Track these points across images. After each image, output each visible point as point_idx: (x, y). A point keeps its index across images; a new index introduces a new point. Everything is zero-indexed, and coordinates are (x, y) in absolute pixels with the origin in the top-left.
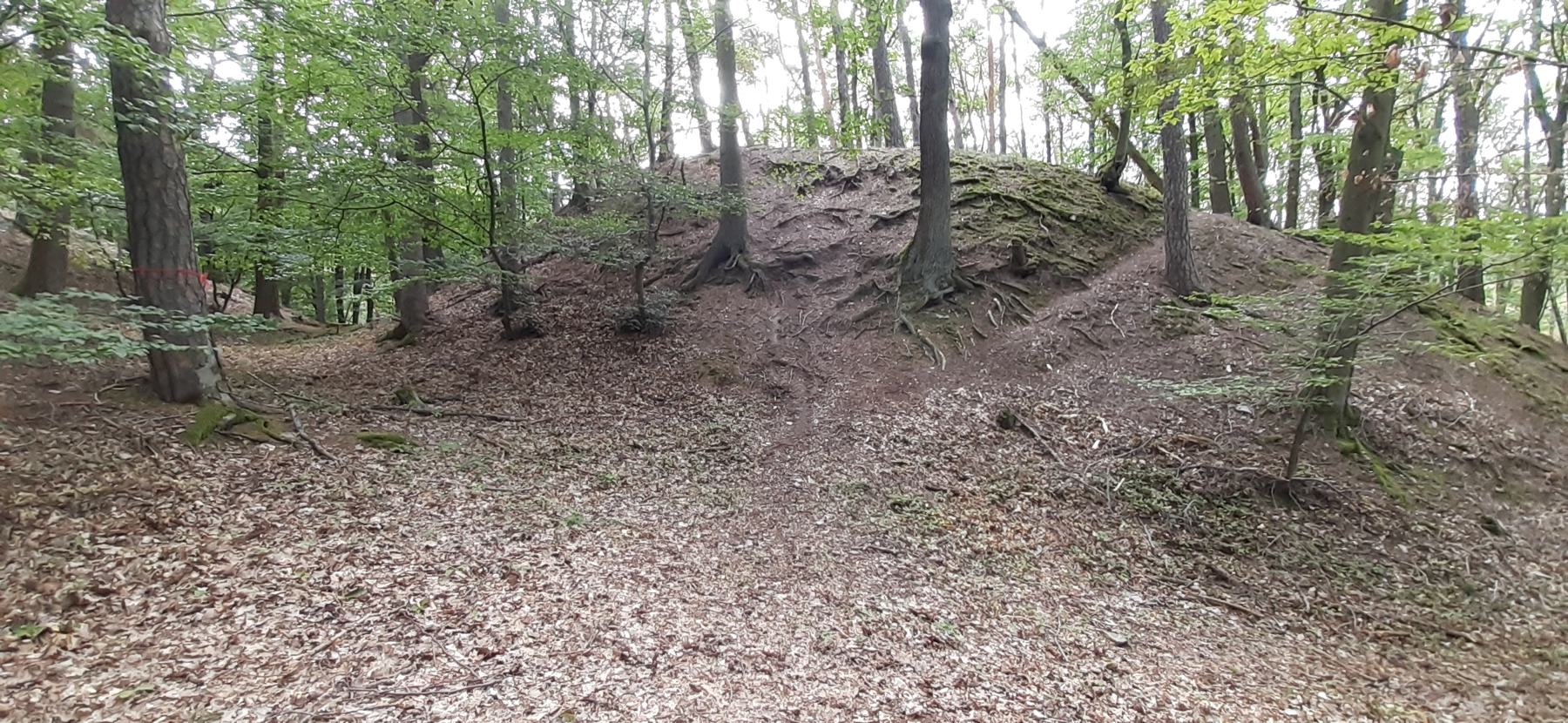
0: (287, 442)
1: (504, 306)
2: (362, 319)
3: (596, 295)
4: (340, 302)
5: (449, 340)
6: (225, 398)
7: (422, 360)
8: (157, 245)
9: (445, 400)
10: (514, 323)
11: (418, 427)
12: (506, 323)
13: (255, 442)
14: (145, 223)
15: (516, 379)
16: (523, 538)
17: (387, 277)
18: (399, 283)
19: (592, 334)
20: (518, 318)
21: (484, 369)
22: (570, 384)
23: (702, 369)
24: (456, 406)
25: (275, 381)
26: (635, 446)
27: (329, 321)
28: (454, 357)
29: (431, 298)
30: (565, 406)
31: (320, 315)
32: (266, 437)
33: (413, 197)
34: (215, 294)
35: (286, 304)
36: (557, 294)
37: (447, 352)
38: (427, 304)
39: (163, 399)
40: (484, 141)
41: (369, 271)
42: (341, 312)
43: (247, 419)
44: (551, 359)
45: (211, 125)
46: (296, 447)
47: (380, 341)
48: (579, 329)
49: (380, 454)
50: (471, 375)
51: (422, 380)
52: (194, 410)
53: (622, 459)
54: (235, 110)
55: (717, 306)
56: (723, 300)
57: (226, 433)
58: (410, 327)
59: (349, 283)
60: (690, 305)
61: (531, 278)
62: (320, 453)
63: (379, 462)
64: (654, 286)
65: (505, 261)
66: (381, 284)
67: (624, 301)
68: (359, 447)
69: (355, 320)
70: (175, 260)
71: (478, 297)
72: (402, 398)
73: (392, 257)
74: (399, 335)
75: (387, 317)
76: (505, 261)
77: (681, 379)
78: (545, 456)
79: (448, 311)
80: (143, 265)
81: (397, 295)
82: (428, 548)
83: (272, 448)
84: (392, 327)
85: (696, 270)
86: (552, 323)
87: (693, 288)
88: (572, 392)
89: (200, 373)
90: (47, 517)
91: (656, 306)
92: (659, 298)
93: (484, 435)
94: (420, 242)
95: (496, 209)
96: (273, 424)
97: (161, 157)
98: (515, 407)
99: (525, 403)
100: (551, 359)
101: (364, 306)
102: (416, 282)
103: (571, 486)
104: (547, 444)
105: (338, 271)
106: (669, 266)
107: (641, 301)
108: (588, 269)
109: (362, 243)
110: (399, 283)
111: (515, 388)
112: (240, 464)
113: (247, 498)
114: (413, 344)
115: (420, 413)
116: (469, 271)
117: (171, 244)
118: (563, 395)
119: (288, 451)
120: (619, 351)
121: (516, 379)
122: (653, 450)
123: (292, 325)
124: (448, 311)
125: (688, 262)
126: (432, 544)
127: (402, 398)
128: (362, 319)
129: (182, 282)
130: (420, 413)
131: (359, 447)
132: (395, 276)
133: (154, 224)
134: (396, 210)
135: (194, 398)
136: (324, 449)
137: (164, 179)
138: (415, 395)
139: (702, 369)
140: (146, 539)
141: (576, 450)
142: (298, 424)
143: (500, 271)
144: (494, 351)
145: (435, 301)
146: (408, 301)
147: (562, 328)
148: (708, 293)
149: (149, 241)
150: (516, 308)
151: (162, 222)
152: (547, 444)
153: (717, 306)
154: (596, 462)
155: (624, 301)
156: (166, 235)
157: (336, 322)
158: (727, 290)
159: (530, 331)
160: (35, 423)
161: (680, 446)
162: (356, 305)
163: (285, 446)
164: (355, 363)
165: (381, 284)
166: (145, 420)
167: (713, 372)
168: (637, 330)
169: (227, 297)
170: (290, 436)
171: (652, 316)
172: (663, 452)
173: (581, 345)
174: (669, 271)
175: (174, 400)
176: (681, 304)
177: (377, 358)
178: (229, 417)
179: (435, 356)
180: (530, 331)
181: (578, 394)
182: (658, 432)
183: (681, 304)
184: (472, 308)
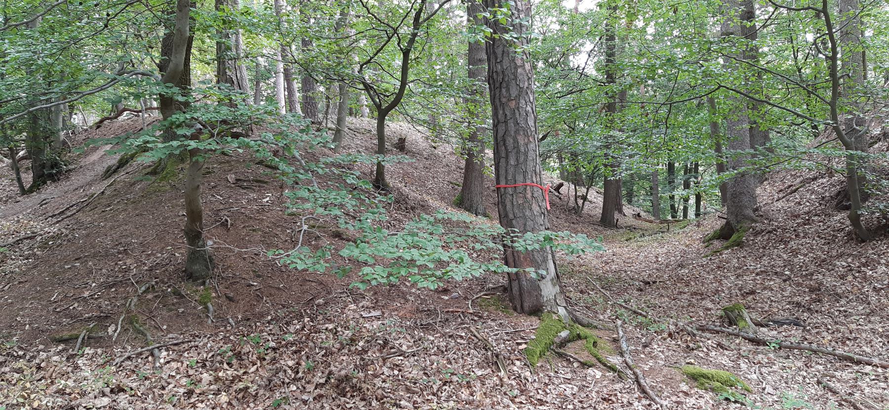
0: (612, 369)
4: (672, 198)
6: (562, 311)
7: (751, 263)
12: (855, 220)
13: (584, 365)
14: (504, 141)
17: (714, 168)
18: (727, 175)
21: (829, 281)
24: (796, 334)
27: (665, 217)
28: (788, 264)
29: (758, 191)
31: (656, 210)
32: (594, 361)
33: (736, 77)
34: (576, 197)
35: (630, 202)
37: (780, 254)
38: (754, 198)
39: (515, 309)
41: (697, 165)
42: (673, 207)
46: (621, 377)
47: (708, 241)
50: (812, 290)
51: (753, 292)
52: (534, 321)
57: (558, 350)
58: (735, 229)
59: (680, 178)
65: (851, 137)
66: (708, 176)
68: (684, 387)
69: (685, 215)
70: (525, 173)
71: (815, 186)
72: (730, 318)
73: (718, 149)
74: (725, 234)
75: (715, 215)
76: (851, 137)
79: (779, 204)
81: (723, 187)
83: (599, 374)
84: (719, 224)
89: (542, 285)
93: (837, 386)
97: (516, 78)
101: (692, 201)
102: (743, 175)
105: (671, 166)
109: (690, 141)
110: (727, 175)
114: (740, 244)
115: (752, 341)
117: (522, 159)
121: (873, 298)
123: (631, 221)
127: (730, 318)
129: (529, 196)
131: (684, 387)
132: (721, 168)
133: (510, 142)
134: (720, 96)
135: (536, 311)
137: (518, 97)
138: (745, 313)
142: (624, 346)
143: (844, 152)
144: (840, 256)
145: (764, 194)
146: (735, 196)
149: (507, 157)
150: (866, 197)
156: (518, 152)
157: (669, 218)
160: (426, 328)
162: (686, 200)
163: (610, 374)
164: (681, 266)
165: (708, 176)
169: (584, 198)
170: (615, 360)
175: (522, 311)
177: (704, 261)
179: (765, 261)
184: (808, 200)
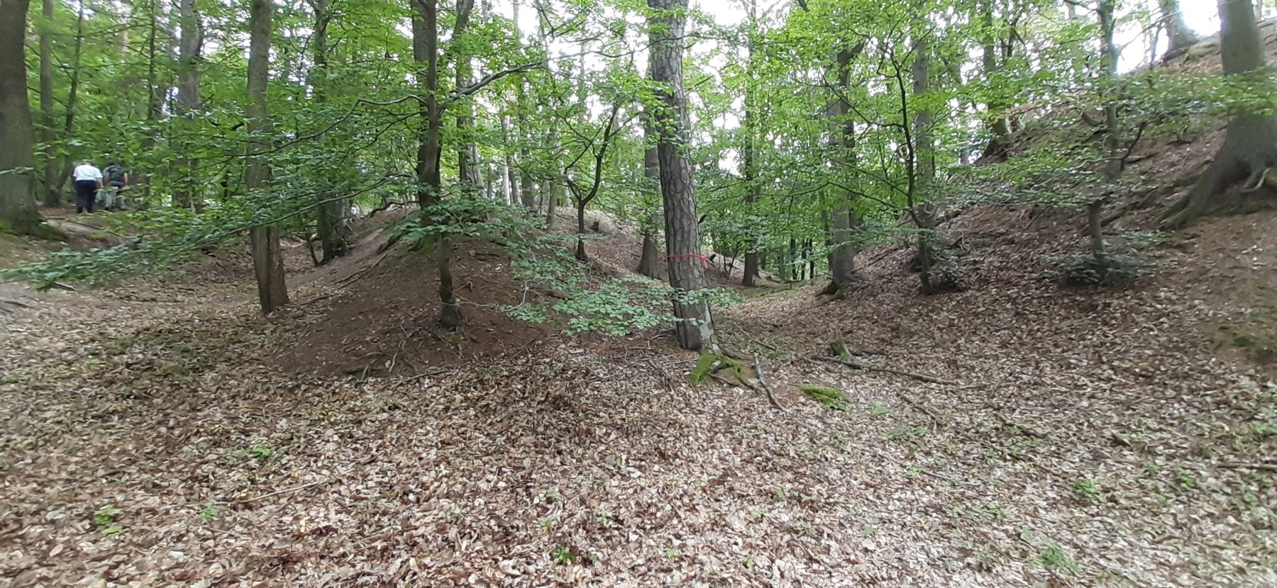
0: (751, 387)
1: (921, 262)
2: (807, 276)
3: (1027, 243)
5: (871, 295)
6: (715, 347)
7: (849, 312)
8: (679, 238)
9: (870, 354)
10: (930, 279)
11: (849, 382)
12: (925, 278)
13: (732, 385)
15: (937, 335)
16: (980, 568)
19: (1026, 288)
20: (935, 273)
21: (905, 323)
22: (1004, 345)
23: (1219, 336)
24: (882, 361)
25: (751, 327)
26: (1116, 442)
28: (875, 311)
30: (1002, 367)
31: (782, 274)
36: (976, 246)
37: (870, 304)
38: (852, 264)
40: (904, 109)
43: (728, 366)
44: (976, 315)
45: (518, 35)
48: (1008, 283)
49: (818, 408)
50: (893, 329)
51: (850, 332)
52: (696, 356)
53: (1097, 457)
54: (735, 145)
55: (1234, 245)
56: (1245, 236)
57: (713, 376)
60: (1180, 247)
61: (945, 232)
62: (773, 403)
63: (817, 417)
64: (1117, 225)
65: (922, 219)
66: (819, 248)
67: (1068, 249)
68: (802, 399)
71: (895, 255)
72: (835, 350)
73: (827, 228)
74: (831, 290)
76: (922, 219)
77: (1177, 348)
78: (986, 436)
79: (870, 269)
80: (672, 254)
81: (830, 257)
82: (866, 550)
83: (741, 392)
84: (828, 283)
85: (1185, 203)
86: (974, 278)
87: (1183, 224)
88: (1008, 355)
90: (609, 435)
91: (1119, 251)
92: (1129, 242)
93: (911, 397)
94: (847, 217)
95: (913, 179)
96: (743, 370)
98: (941, 366)
99: (952, 363)
100: (976, 315)
101: (808, 266)
102: (844, 247)
103: (1029, 489)
104: (987, 422)
106: (1134, 200)
107: (1097, 246)
108: (1013, 216)
110: (831, 248)
111: (937, 345)
112: (720, 405)
113: (722, 438)
114: (842, 298)
115: (851, 366)
116: (891, 234)
118: (997, 358)
119: (752, 397)
120: (1067, 308)
121: (937, 335)
122: (1151, 452)
124: (870, 269)
125: (1169, 191)
126: (872, 547)
127: (835, 350)
128: (807, 276)
130: (851, 366)
135: (697, 348)
136: (776, 396)
137: (682, 192)
138: (845, 346)
139: (1219, 336)
140: (656, 467)
141: (1026, 433)
142: (760, 371)
144: (913, 305)
145: (859, 261)
146: (839, 263)
147: (987, 282)
148: (1212, 230)
150: (933, 262)
151: (681, 223)
152: (987, 422)
153: (1234, 245)
154: (1057, 454)
155: (1068, 249)
158: (1252, 222)
159: (950, 285)
160: (617, 361)
161: (1202, 453)
162: (804, 266)
163: (749, 391)
164: (800, 314)
165: (819, 248)
166: (668, 363)
167: (1242, 342)
168: (1091, 284)
170: (753, 381)
171: (1117, 265)
172: (1170, 457)
173: (1013, 301)
174: (1135, 206)
175: (687, 348)
176: (1162, 246)
177: (816, 310)
178: (717, 363)
179: (860, 309)
180: (950, 285)
181: (1016, 358)
182: (1152, 423)
183: (1162, 246)
184: (891, 265)
